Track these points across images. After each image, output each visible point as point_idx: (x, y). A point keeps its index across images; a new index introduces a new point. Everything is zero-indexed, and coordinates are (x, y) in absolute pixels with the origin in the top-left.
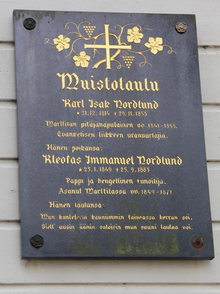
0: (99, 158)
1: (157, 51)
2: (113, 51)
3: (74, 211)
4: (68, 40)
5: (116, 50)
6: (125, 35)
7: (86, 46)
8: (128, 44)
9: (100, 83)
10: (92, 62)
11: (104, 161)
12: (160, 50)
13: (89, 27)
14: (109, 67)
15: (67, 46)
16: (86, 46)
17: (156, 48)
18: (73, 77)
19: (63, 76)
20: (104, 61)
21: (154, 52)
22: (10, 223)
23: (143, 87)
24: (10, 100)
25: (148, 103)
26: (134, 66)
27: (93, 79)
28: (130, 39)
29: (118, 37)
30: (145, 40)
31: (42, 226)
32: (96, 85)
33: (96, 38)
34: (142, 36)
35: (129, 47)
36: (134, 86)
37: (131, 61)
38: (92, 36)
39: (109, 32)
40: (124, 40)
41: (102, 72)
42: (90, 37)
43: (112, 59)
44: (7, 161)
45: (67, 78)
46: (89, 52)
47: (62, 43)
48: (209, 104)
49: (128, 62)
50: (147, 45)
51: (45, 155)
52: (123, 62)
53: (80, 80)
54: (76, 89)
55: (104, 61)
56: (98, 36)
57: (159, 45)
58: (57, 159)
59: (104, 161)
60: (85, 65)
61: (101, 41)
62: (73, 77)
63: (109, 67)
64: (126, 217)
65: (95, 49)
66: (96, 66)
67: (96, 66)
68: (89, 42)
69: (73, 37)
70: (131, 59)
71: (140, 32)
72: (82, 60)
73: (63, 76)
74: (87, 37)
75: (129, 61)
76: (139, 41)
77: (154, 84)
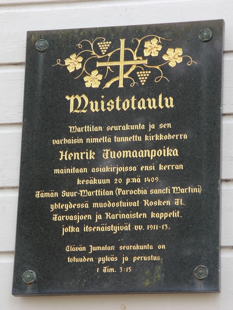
0: (148, 108)
1: (175, 64)
2: (127, 68)
3: (92, 211)
4: (80, 59)
5: (130, 66)
6: (142, 48)
7: (99, 64)
8: (144, 58)
9: (110, 103)
10: (103, 82)
11: (96, 205)
12: (179, 62)
13: (104, 43)
14: (121, 85)
15: (79, 66)
16: (99, 64)
17: (174, 60)
18: (82, 99)
19: (72, 99)
20: (115, 80)
21: (172, 64)
22: (18, 66)
23: (157, 104)
24: (14, 63)
25: (103, 207)
26: (150, 79)
27: (104, 99)
28: (146, 53)
29: (134, 52)
30: (163, 52)
31: (63, 193)
32: (106, 107)
33: (109, 55)
34: (160, 48)
35: (145, 62)
36: (147, 104)
37: (146, 76)
38: (106, 53)
39: (125, 47)
40: (140, 53)
41: (113, 93)
42: (103, 53)
43: (126, 76)
44: (11, 66)
45: (76, 101)
46: (102, 70)
47: (73, 63)
48: (230, 114)
49: (143, 78)
50: (165, 58)
51: (70, 96)
52: (137, 79)
53: (89, 101)
54: (84, 111)
55: (115, 80)
56: (112, 53)
57: (179, 56)
58: (69, 155)
59: (96, 205)
60: (96, 85)
61: (116, 57)
62: (82, 99)
63: (121, 85)
64: (145, 227)
65: (108, 67)
66: (108, 85)
67: (108, 85)
68: (101, 60)
69: (85, 56)
70: (146, 74)
71: (159, 44)
72: (93, 80)
73: (72, 99)
74: (100, 54)
75: (143, 76)
76: (156, 54)
77: (169, 100)
